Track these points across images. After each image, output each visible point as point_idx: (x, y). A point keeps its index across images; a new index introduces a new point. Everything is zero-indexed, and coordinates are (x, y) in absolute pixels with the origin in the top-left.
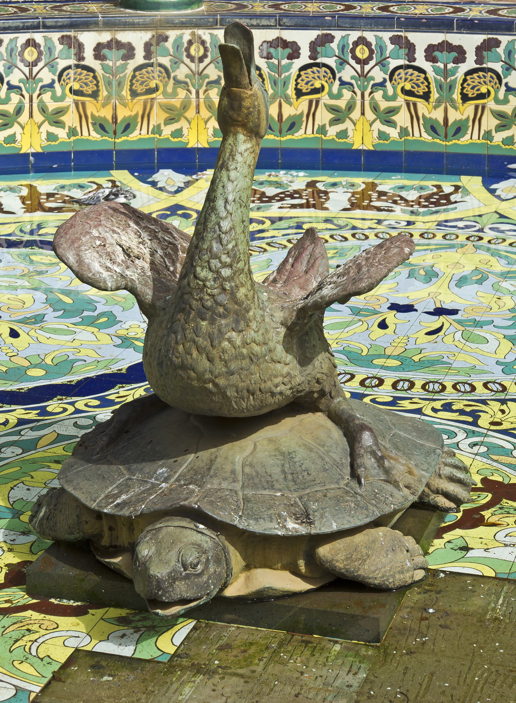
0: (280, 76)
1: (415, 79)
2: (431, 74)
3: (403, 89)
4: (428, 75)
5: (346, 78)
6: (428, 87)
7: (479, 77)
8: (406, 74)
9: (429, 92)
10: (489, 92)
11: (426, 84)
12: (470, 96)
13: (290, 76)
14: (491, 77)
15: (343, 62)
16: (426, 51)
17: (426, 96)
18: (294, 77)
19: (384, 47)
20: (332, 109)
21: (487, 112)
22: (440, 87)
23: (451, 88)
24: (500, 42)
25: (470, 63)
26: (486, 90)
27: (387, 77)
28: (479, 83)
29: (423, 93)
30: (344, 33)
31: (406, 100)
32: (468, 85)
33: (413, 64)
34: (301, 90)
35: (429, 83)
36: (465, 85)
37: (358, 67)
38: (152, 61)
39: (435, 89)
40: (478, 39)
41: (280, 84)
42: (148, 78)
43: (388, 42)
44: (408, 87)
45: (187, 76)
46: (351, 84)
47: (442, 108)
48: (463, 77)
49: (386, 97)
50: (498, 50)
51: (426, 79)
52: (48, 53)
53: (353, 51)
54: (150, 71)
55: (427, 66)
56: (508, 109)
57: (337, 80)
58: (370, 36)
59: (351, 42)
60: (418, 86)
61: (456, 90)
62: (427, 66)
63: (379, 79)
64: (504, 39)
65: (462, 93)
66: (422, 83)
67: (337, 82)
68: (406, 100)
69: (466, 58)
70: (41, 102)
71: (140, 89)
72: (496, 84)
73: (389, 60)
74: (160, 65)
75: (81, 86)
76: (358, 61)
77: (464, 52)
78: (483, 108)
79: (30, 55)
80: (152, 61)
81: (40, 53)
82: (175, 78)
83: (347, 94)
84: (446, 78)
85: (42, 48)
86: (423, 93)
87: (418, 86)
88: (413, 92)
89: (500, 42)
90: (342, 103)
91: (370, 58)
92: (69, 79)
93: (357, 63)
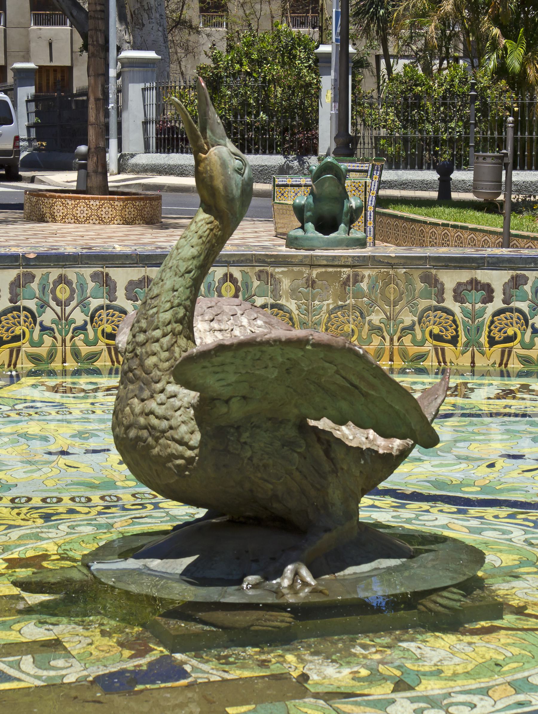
0: (473, 322)
1: (444, 321)
2: (459, 316)
3: (431, 332)
4: (456, 318)
5: (47, 323)
6: (456, 330)
7: (14, 318)
8: (435, 317)
9: (457, 336)
10: (515, 334)
11: (454, 327)
12: (497, 339)
13: (483, 322)
14: (518, 318)
15: (43, 305)
16: (455, 291)
17: (454, 341)
18: (487, 322)
19: (249, 284)
20: (35, 358)
21: (22, 354)
22: (468, 331)
23: (479, 329)
24: (527, 279)
25: (498, 303)
26: (513, 332)
27: (88, 319)
28: (507, 325)
29: (452, 337)
30: (45, 271)
31: (107, 344)
32: (496, 327)
33: (442, 304)
34: (494, 338)
35: (457, 326)
36: (492, 327)
37: (58, 309)
38: (347, 303)
39: (463, 332)
40: (505, 276)
41: (473, 332)
42: (507, 325)
43: (89, 280)
44: (436, 330)
45: (53, 322)
46: (53, 330)
47: (469, 354)
48: (491, 318)
49: (87, 343)
50: (525, 287)
51: (454, 321)
52: (246, 289)
53: (53, 291)
54: (509, 318)
55: (456, 308)
56: (532, 353)
57: (529, 327)
58: (236, 272)
59: (51, 280)
60: (447, 330)
61: (483, 333)
62: (456, 308)
63: (79, 322)
64: (531, 275)
65: (489, 337)
66: (451, 326)
67: (38, 328)
68: (107, 344)
69: (493, 297)
70: (74, 345)
71: (498, 336)
72: (31, 324)
73: (90, 299)
74: (25, 309)
75: (441, 331)
76: (59, 303)
77: (492, 291)
78: (19, 350)
79: (63, 293)
80: (347, 303)
81: (73, 291)
82: (41, 324)
83: (48, 340)
84: (473, 322)
85: (239, 284)
86: (452, 337)
87: (447, 330)
88: (442, 336)
89: (527, 279)
90: (43, 351)
91: (71, 298)
92: (429, 321)
93: (58, 305)
